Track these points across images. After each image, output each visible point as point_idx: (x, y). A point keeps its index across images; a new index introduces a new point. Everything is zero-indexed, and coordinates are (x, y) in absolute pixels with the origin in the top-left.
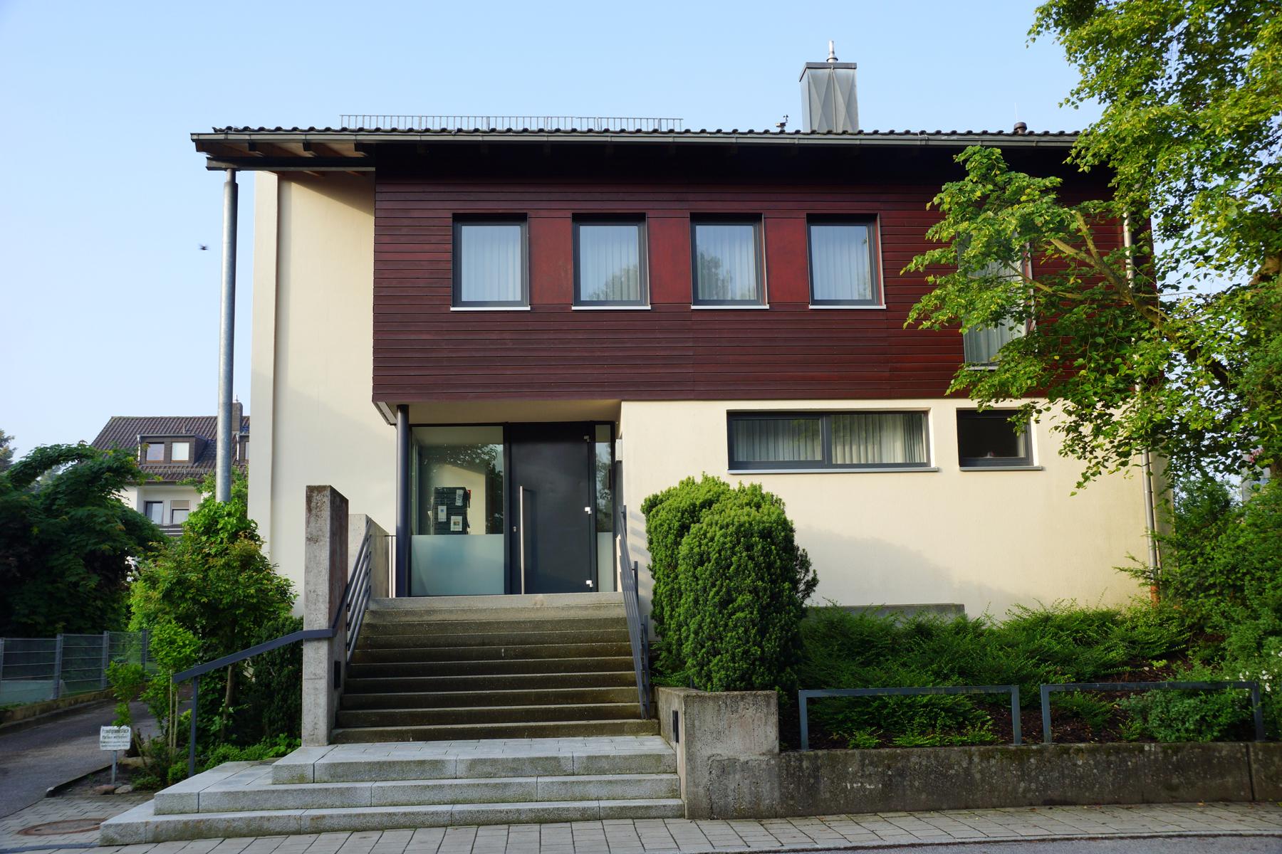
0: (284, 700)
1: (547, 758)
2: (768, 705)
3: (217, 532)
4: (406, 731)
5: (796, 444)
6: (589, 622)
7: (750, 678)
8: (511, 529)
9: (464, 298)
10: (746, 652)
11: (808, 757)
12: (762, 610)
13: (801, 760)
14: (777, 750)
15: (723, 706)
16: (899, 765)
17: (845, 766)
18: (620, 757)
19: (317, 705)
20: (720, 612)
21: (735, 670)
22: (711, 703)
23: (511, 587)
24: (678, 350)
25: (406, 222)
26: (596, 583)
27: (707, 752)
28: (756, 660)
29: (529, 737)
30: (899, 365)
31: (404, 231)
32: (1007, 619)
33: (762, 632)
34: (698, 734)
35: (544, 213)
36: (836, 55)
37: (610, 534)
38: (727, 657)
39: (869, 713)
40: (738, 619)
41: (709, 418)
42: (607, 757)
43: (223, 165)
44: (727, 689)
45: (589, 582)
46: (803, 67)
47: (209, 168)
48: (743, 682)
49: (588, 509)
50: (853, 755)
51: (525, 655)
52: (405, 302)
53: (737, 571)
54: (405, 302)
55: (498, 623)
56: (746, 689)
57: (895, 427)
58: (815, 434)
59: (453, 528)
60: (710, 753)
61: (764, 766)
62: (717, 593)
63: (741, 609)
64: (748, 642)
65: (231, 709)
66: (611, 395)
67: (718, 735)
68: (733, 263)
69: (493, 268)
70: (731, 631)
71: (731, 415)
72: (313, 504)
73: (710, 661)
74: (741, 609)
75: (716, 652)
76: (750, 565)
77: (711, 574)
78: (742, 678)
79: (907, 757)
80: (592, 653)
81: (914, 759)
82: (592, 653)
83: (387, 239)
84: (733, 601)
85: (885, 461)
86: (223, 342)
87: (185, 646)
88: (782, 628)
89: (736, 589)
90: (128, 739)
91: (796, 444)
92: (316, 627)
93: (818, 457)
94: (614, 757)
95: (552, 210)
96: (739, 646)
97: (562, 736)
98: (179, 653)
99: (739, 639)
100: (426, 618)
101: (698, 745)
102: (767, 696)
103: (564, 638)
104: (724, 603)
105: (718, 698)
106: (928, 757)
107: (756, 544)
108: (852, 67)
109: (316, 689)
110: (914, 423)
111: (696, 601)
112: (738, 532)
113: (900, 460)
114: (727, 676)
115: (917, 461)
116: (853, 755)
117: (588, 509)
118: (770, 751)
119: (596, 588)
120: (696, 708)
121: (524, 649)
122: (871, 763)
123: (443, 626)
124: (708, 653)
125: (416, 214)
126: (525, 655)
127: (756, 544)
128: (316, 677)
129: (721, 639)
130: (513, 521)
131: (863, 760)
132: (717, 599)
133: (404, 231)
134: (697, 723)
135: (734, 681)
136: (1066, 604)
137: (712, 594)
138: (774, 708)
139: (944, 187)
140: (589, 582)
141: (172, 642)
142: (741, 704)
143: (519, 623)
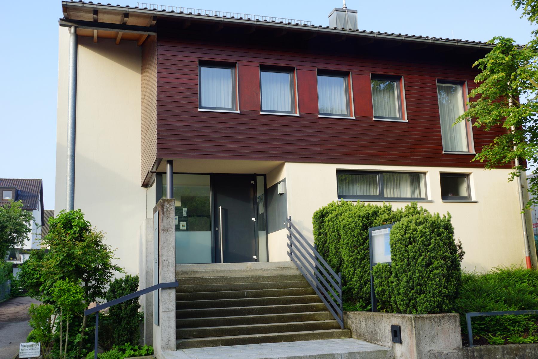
0: (128, 323)
1: (327, 355)
2: (455, 321)
3: (71, 227)
4: (218, 341)
5: (365, 188)
6: (274, 277)
7: (442, 306)
8: (215, 229)
9: (203, 105)
10: (440, 292)
11: (477, 350)
12: (448, 268)
13: (473, 352)
14: (461, 346)
15: (434, 322)
16: (521, 354)
17: (495, 355)
18: (365, 352)
19: (169, 327)
20: (425, 270)
21: (434, 302)
22: (427, 321)
23: (216, 259)
24: (310, 138)
25: (174, 62)
26: (258, 257)
27: (427, 349)
28: (445, 296)
29: (285, 341)
30: (414, 149)
31: (173, 67)
32: (480, 274)
33: (447, 281)
34: (422, 338)
35: (245, 63)
36: (347, 6)
37: (264, 232)
38: (429, 295)
39: (484, 324)
40: (435, 274)
41: (329, 171)
42: (359, 353)
43: (70, 24)
44: (429, 313)
45: (255, 257)
46: (333, 9)
47: (61, 25)
48: (439, 309)
49: (254, 219)
50: (498, 348)
51: (257, 295)
52: (174, 105)
53: (434, 248)
54: (174, 105)
55: (235, 278)
56: (439, 313)
57: (406, 180)
58: (374, 183)
59: (181, 228)
60: (428, 349)
61: (456, 356)
62: (423, 260)
63: (437, 268)
64: (441, 286)
65: (87, 329)
66: (277, 159)
67: (432, 339)
68: (334, 98)
69: (218, 91)
70: (431, 280)
71: (339, 172)
72: (165, 210)
73: (417, 297)
74: (437, 268)
75: (422, 292)
76: (442, 244)
77: (419, 248)
78: (438, 307)
79: (524, 349)
80: (291, 293)
81: (528, 351)
82: (291, 293)
83: (163, 71)
84: (432, 263)
85: (402, 197)
86: (70, 121)
87: (77, 293)
88: (456, 279)
89: (433, 258)
90: (39, 350)
91: (365, 188)
92: (168, 281)
93: (378, 194)
94: (363, 352)
95: (249, 64)
96: (436, 289)
97: (302, 340)
98: (74, 297)
99: (436, 285)
100: (193, 276)
101: (423, 345)
102: (454, 316)
103: (273, 286)
104: (428, 264)
105: (431, 318)
106: (535, 349)
107: (443, 232)
108: (355, 12)
109: (169, 317)
110: (415, 178)
111: (408, 264)
112: (432, 226)
113: (409, 196)
114: (431, 306)
115: (416, 197)
116: (498, 348)
117: (254, 219)
118: (458, 347)
119: (257, 260)
120: (420, 323)
121: (257, 292)
122: (508, 353)
123: (205, 280)
124: (416, 293)
125: (179, 58)
126: (257, 295)
127: (443, 232)
128: (169, 310)
129: (426, 285)
130: (216, 224)
131: (503, 352)
132: (424, 263)
133: (173, 67)
134: (421, 332)
135: (434, 308)
136: (518, 267)
137: (419, 260)
138: (458, 323)
139: (486, 56)
140: (255, 257)
141: (69, 291)
142: (442, 321)
143: (245, 278)
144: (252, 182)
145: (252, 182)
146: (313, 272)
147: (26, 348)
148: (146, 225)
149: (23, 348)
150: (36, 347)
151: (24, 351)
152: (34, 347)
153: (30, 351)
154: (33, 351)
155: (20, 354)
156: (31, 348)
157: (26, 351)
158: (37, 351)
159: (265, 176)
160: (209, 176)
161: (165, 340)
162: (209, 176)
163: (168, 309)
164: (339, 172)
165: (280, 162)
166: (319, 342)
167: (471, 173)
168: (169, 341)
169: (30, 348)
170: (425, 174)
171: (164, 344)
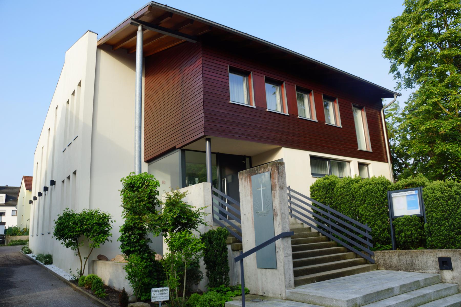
19: (289, 269)
69: (240, 92)
72: (280, 171)
90: (168, 295)
109: (289, 261)
121: (296, 240)
144: (244, 161)
145: (244, 161)
146: (315, 225)
147: (157, 293)
148: (204, 188)
149: (155, 293)
150: (166, 292)
151: (155, 296)
152: (163, 292)
153: (160, 295)
154: (163, 295)
155: (152, 299)
156: (162, 292)
157: (157, 296)
158: (166, 295)
159: (250, 158)
160: (215, 155)
161: (288, 280)
162: (215, 155)
163: (288, 254)
164: (312, 157)
165: (278, 146)
166: (364, 275)
167: (370, 164)
168: (290, 281)
169: (160, 293)
170: (349, 162)
171: (287, 284)
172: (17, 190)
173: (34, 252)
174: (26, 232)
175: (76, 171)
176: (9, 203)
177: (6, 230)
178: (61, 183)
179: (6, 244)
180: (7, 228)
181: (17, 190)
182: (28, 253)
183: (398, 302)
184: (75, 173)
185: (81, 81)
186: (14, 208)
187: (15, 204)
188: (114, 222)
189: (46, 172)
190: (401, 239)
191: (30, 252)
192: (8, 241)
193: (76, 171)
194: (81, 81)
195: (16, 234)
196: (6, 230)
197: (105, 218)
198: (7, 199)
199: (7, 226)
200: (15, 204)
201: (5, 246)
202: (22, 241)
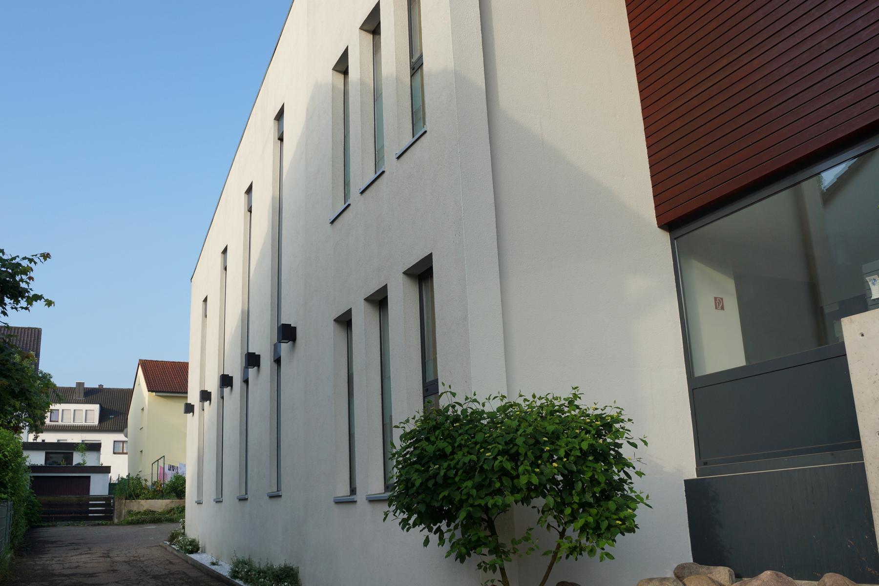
172: (126, 395)
173: (208, 549)
174: (177, 489)
175: (428, 261)
176: (108, 423)
177: (112, 486)
178: (331, 330)
179: (116, 521)
180: (114, 479)
181: (126, 395)
182: (192, 552)
183: (790, 579)
184: (422, 274)
185: (283, 105)
186: (120, 437)
187: (121, 427)
188: (640, 444)
189: (246, 317)
190: (631, 441)
191: (195, 547)
192: (121, 513)
193: (428, 261)
194: (283, 105)
195: (137, 496)
196: (112, 486)
197: (608, 426)
198: (104, 415)
199: (114, 476)
200: (121, 427)
201: (113, 524)
202: (154, 512)
